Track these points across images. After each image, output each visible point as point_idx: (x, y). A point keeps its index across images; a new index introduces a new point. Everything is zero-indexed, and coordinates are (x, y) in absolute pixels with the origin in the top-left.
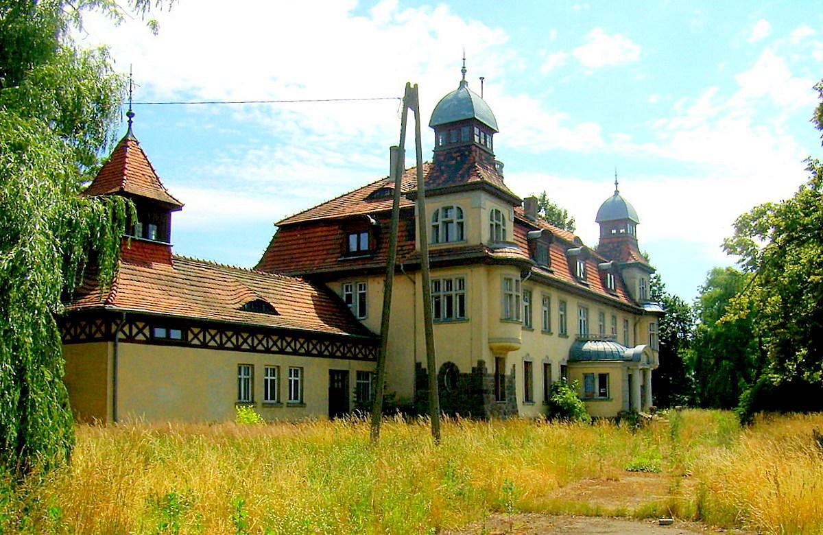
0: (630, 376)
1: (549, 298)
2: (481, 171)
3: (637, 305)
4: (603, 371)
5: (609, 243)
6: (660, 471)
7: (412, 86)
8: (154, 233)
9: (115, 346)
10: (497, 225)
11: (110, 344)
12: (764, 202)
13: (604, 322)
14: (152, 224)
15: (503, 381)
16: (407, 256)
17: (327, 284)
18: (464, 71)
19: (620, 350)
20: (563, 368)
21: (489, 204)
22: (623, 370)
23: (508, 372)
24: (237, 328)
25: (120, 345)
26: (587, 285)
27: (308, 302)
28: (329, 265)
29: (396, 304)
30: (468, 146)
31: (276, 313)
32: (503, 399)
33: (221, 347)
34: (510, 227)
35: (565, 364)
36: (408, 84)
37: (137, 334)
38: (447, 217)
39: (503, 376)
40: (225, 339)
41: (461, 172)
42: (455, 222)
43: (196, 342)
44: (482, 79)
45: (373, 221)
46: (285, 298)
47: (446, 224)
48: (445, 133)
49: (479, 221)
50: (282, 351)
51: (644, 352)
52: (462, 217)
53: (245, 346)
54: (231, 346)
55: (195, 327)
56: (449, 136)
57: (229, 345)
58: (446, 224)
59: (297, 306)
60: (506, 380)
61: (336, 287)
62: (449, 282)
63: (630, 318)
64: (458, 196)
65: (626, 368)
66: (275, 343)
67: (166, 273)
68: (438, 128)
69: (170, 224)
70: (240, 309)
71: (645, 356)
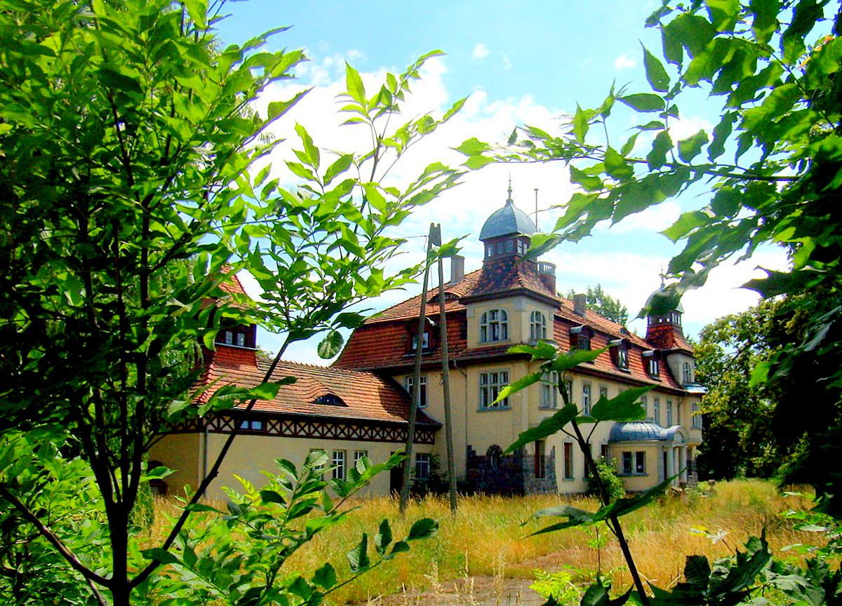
0: (665, 455)
1: (589, 386)
2: (523, 278)
3: (680, 387)
4: (640, 449)
5: (656, 331)
6: (823, 550)
7: (436, 226)
8: (242, 340)
9: (205, 436)
10: (537, 325)
11: (202, 435)
12: (726, 315)
13: (658, 406)
14: (241, 333)
15: (543, 461)
16: (460, 353)
17: (394, 378)
18: (510, 191)
19: (656, 430)
20: (603, 447)
21: (529, 307)
22: (657, 448)
23: (548, 453)
24: (309, 420)
25: (209, 434)
26: (629, 373)
27: (375, 394)
28: (396, 361)
29: (452, 397)
30: (513, 257)
31: (345, 405)
32: (543, 475)
33: (295, 435)
34: (550, 325)
35: (606, 443)
36: (433, 224)
37: (224, 426)
38: (493, 318)
39: (543, 457)
40: (298, 429)
41: (505, 280)
42: (500, 324)
43: (273, 431)
44: (536, 190)
45: (432, 322)
46: (354, 391)
47: (494, 325)
48: (492, 245)
49: (521, 323)
50: (348, 438)
51: (678, 432)
52: (506, 319)
53: (316, 434)
54: (318, 435)
55: (273, 419)
56: (496, 248)
57: (302, 433)
58: (494, 325)
59: (364, 398)
60: (546, 460)
61: (401, 380)
62: (495, 376)
63: (674, 400)
64: (501, 301)
65: (660, 447)
66: (342, 431)
67: (252, 374)
68: (487, 241)
69: (255, 336)
70: (313, 402)
71: (680, 436)
